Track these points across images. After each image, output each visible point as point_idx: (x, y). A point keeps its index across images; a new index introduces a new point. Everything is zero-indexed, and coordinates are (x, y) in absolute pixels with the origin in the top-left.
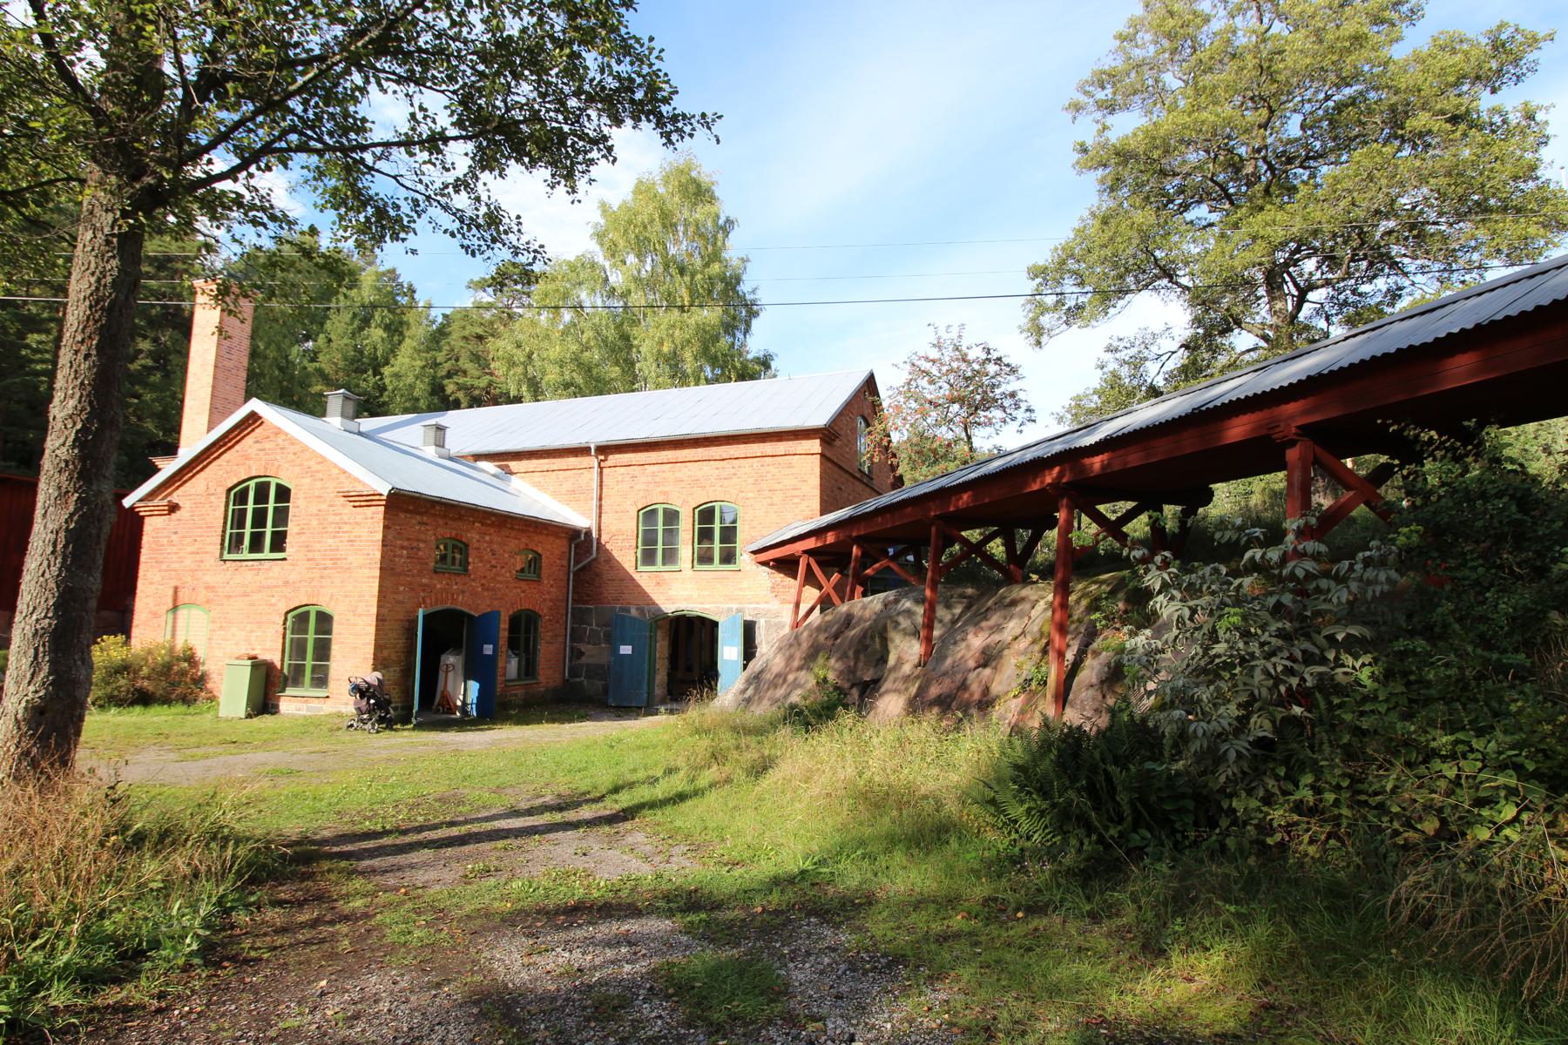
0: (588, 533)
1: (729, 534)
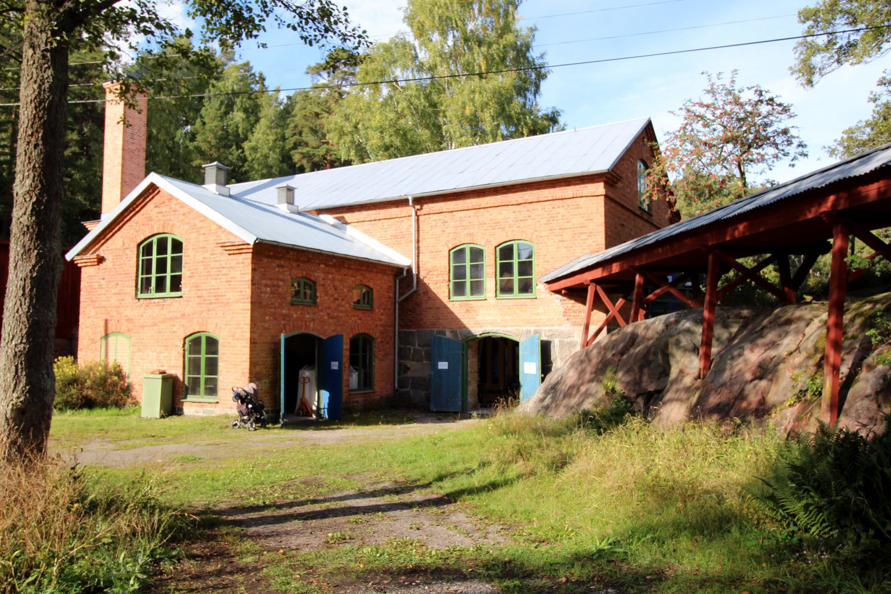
1: (526, 268)
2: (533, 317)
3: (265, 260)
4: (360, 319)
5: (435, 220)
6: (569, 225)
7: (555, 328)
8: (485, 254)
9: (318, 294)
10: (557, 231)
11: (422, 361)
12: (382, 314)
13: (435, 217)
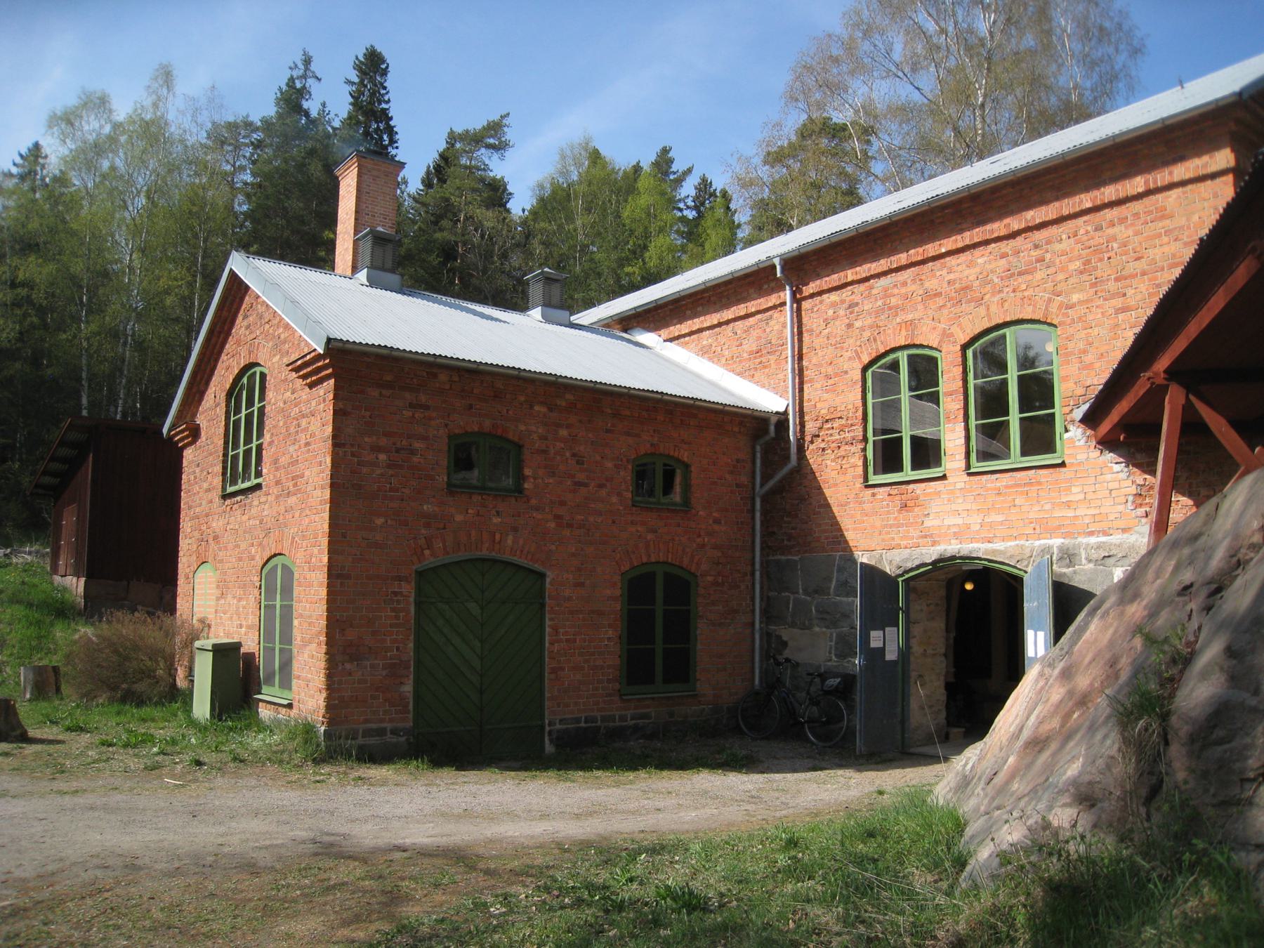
0: (782, 420)
1: (1038, 390)
2: (1058, 513)
3: (375, 393)
4: (654, 531)
5: (834, 305)
6: (1141, 265)
7: (1116, 538)
8: (941, 366)
9: (527, 472)
10: (1112, 286)
11: (809, 628)
12: (717, 521)
13: (834, 297)
